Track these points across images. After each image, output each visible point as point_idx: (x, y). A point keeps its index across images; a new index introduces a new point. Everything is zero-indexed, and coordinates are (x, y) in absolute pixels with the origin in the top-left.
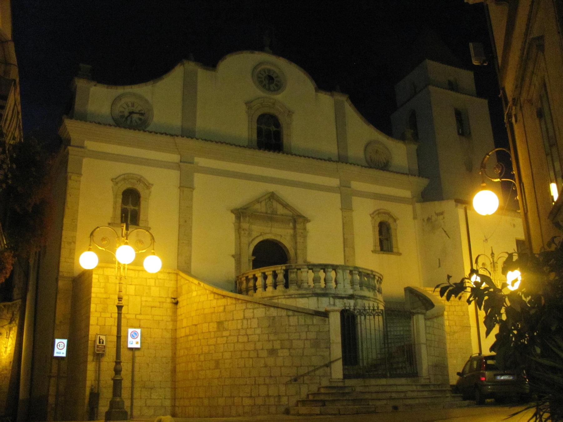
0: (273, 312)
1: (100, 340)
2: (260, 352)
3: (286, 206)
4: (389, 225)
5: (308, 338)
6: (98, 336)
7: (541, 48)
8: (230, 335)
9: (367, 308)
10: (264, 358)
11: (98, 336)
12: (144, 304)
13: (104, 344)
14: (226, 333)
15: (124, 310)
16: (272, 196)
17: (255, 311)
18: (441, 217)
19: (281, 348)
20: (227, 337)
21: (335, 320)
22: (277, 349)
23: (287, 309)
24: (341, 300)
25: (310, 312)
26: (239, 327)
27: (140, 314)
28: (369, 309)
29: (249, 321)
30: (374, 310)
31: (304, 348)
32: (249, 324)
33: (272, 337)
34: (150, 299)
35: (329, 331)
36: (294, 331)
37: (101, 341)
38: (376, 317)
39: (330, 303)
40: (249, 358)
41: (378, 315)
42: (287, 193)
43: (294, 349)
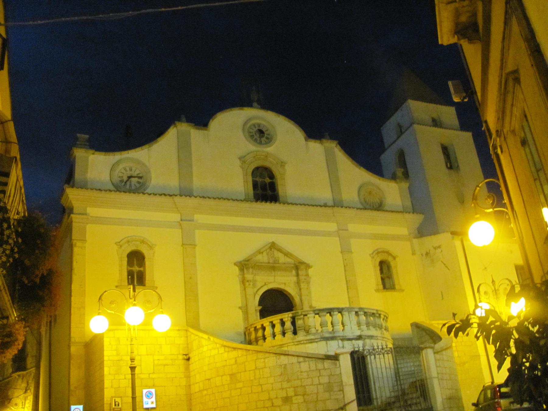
0: (284, 360)
1: (115, 402)
2: (274, 401)
3: (287, 254)
4: (389, 263)
5: (321, 382)
6: (114, 399)
7: (517, 80)
8: (244, 387)
9: (376, 347)
10: (279, 406)
11: (114, 399)
12: (156, 362)
13: (120, 406)
14: (240, 385)
15: (137, 371)
16: (273, 246)
17: (266, 360)
18: (439, 250)
19: (296, 395)
20: (241, 388)
21: (346, 363)
22: (292, 397)
23: (297, 356)
24: (349, 342)
25: (320, 357)
26: (252, 378)
27: (154, 373)
28: (378, 348)
29: (261, 371)
30: (383, 349)
31: (317, 393)
32: (261, 373)
33: (285, 385)
34: (162, 357)
35: (341, 373)
36: (307, 377)
37: (117, 403)
38: (386, 355)
39: (338, 345)
40: (264, 407)
41: (388, 354)
42: (283, 241)
43: (308, 395)
